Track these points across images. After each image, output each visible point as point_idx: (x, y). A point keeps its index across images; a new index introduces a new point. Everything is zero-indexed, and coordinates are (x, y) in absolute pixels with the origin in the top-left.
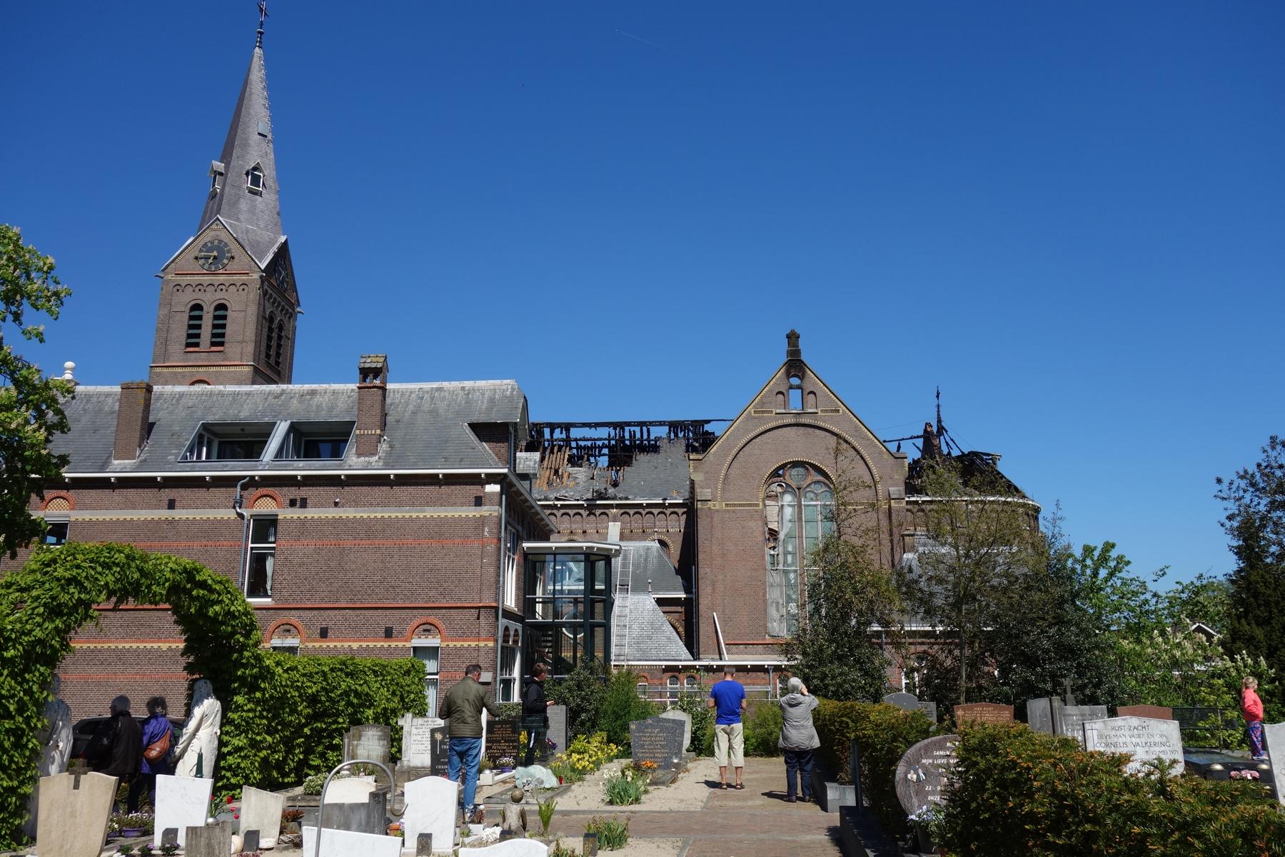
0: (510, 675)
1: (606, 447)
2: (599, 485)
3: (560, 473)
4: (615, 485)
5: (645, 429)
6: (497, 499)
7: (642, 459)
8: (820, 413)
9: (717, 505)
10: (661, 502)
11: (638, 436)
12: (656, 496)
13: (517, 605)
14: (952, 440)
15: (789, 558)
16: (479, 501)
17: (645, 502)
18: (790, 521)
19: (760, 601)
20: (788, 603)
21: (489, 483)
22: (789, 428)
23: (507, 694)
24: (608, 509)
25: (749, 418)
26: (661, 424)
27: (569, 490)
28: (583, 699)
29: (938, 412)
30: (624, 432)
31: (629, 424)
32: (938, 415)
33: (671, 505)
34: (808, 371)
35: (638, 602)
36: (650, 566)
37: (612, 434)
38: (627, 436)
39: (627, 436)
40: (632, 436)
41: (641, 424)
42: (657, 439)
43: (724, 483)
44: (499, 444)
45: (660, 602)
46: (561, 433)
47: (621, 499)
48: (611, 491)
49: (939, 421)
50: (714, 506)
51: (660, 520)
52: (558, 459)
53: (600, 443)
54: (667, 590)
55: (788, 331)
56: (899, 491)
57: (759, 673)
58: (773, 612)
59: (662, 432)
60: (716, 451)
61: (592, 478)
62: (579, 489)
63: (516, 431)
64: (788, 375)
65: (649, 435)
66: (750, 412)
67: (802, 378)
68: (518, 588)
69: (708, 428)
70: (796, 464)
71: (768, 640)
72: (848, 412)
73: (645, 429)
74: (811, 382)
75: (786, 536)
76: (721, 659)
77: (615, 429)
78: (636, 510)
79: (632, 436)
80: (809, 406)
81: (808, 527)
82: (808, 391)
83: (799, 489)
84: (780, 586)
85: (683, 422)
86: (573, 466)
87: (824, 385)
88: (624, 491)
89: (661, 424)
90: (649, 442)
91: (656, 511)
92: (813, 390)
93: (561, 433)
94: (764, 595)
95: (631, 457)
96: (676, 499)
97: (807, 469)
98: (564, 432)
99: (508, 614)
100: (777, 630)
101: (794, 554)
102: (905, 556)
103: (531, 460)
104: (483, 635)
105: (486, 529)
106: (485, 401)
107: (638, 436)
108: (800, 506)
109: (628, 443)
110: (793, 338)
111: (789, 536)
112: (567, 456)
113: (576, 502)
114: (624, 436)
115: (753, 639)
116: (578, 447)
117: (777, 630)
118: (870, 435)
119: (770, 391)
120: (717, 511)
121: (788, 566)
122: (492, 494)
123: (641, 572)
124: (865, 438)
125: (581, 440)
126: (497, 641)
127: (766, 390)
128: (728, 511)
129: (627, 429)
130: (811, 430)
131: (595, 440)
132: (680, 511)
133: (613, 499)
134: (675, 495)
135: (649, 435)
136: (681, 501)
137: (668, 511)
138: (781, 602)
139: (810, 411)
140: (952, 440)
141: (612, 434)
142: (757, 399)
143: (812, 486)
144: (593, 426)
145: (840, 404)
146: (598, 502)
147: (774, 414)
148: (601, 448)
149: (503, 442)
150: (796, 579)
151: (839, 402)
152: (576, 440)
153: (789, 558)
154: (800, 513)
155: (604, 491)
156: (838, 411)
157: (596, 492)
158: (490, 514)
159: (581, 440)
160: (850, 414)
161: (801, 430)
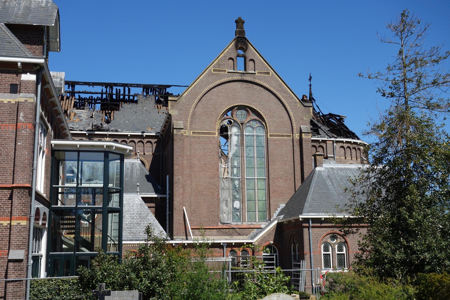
0: (38, 252)
1: (99, 99)
2: (97, 122)
3: (68, 113)
4: (108, 122)
5: (127, 89)
6: (33, 88)
7: (126, 107)
8: (257, 74)
9: (187, 133)
10: (141, 134)
11: (122, 92)
12: (137, 130)
13: (45, 192)
14: (317, 106)
15: (235, 170)
16: (14, 89)
17: (129, 134)
18: (236, 145)
19: (215, 199)
20: (233, 201)
21: (25, 73)
22: (236, 83)
23: (36, 272)
24: (103, 137)
25: (210, 74)
26: (138, 86)
27: (75, 124)
28: (152, 280)
29: (310, 89)
30: (112, 90)
31: (116, 85)
32: (310, 91)
33: (148, 137)
34: (250, 45)
35: (129, 199)
36: (135, 176)
37: (104, 91)
38: (114, 92)
39: (114, 92)
40: (118, 94)
41: (124, 85)
42: (136, 95)
43: (192, 118)
44: (34, 46)
45: (146, 200)
46: (69, 88)
47: (112, 131)
48: (105, 126)
49: (311, 94)
50: (185, 133)
51: (139, 146)
52: (67, 104)
53: (95, 96)
54: (147, 192)
55: (237, 18)
56: (307, 128)
57: (216, 249)
58: (223, 207)
59: (139, 90)
60: (187, 95)
61: (92, 117)
62: (82, 123)
63: (48, 33)
64: (237, 47)
65: (129, 92)
66: (210, 70)
67: (245, 50)
68: (46, 177)
69: (168, 90)
70: (240, 107)
71: (220, 226)
72: (275, 74)
73: (127, 89)
74: (251, 53)
75: (233, 155)
76: (187, 239)
77: (106, 87)
78: (123, 139)
79: (118, 94)
80: (250, 69)
81: (248, 150)
82: (250, 58)
83: (242, 124)
84: (228, 189)
85: (153, 85)
86: (77, 109)
87: (260, 55)
88: (115, 126)
89: (138, 86)
90: (129, 98)
91: (136, 140)
92: (252, 58)
93: (69, 88)
94: (218, 195)
95: (119, 105)
96: (151, 133)
97: (248, 111)
98: (71, 88)
99: (39, 197)
100: (226, 219)
101: (238, 168)
102: (317, 169)
103: (57, 78)
104: (15, 213)
105: (21, 114)
106: (22, 9)
107: (122, 92)
108: (242, 135)
109: (114, 97)
110: (239, 22)
111: (235, 155)
112: (73, 102)
113: (80, 132)
114: (112, 92)
115: (210, 225)
116: (80, 98)
117: (226, 219)
118: (289, 90)
119: (224, 57)
120: (187, 136)
121: (234, 175)
122: (28, 82)
123: (128, 180)
124: (285, 92)
125: (82, 93)
126: (30, 220)
127: (221, 56)
128: (194, 137)
129: (115, 88)
130: (251, 85)
131: (92, 93)
132: (153, 141)
133: (107, 131)
134: (150, 130)
135: (129, 92)
136: (154, 134)
137: (145, 141)
138: (229, 199)
139: (250, 72)
140: (317, 106)
141: (104, 91)
142: (216, 62)
143: (251, 122)
144: (91, 85)
145: (270, 69)
146: (96, 133)
147: (226, 73)
148: (96, 100)
149: (38, 45)
150: (239, 184)
151: (269, 68)
152: (79, 92)
153: (235, 170)
154: (242, 140)
155: (100, 126)
156: (269, 73)
157: (95, 126)
158: (26, 101)
159: (82, 93)
160: (276, 76)
161: (245, 84)
